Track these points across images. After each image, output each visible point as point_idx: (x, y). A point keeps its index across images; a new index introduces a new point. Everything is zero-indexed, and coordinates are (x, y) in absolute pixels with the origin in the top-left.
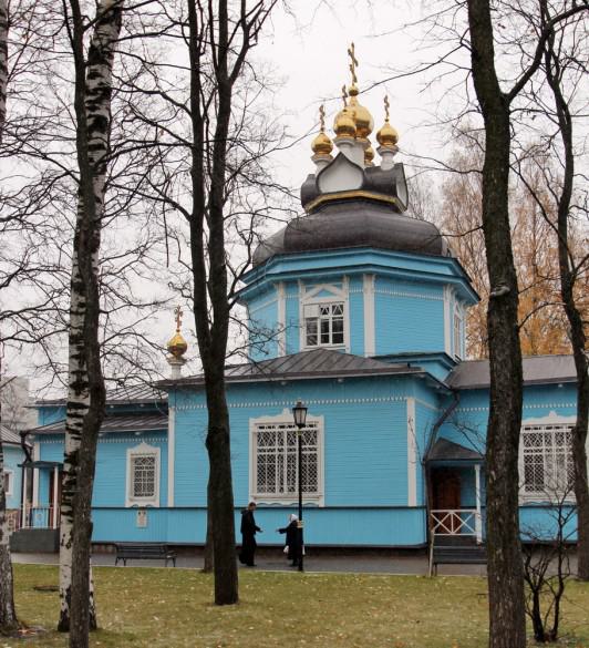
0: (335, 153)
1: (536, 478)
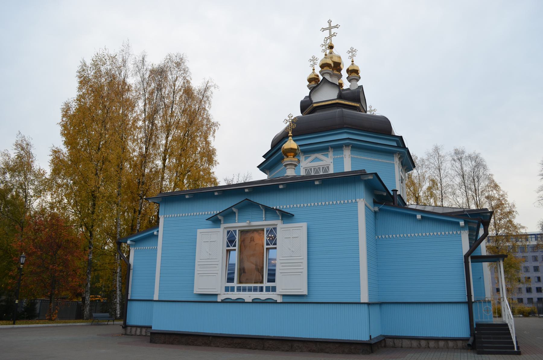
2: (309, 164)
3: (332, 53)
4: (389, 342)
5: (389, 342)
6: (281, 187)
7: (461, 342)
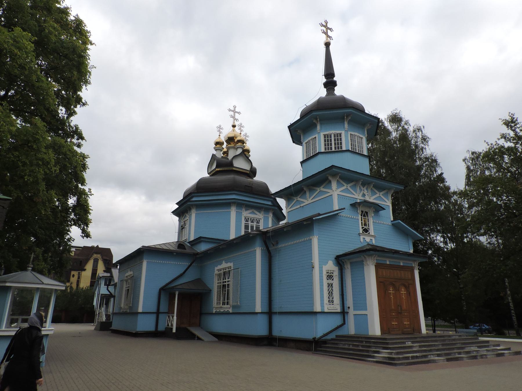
3: (235, 130)
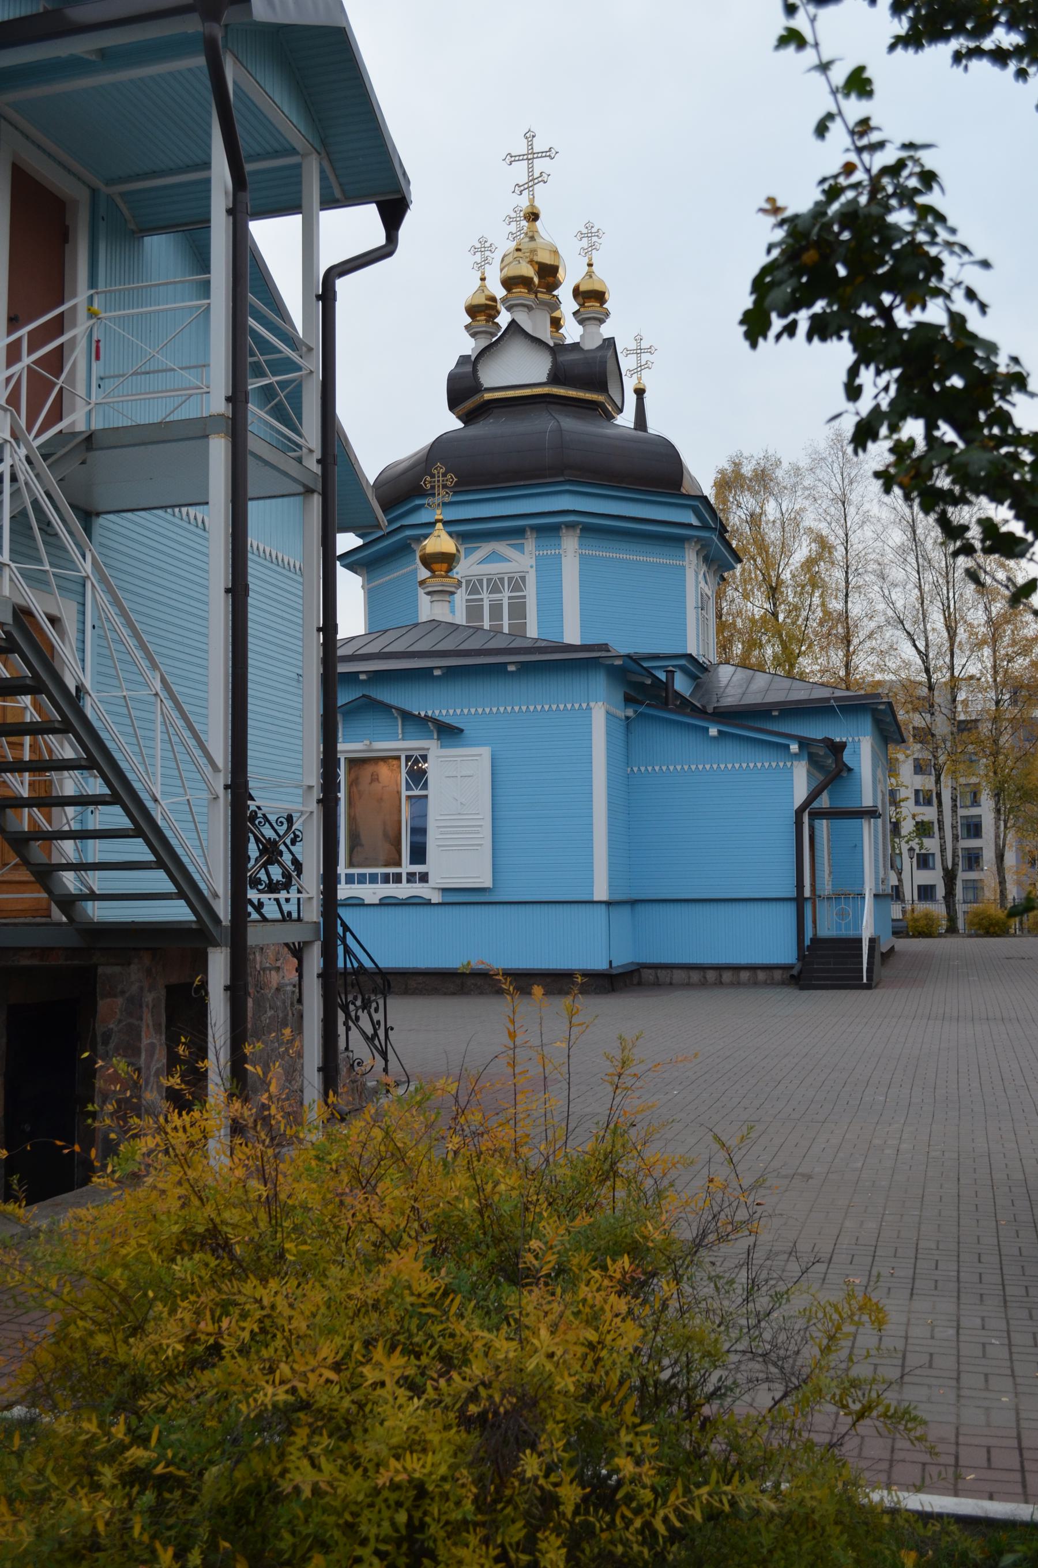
0: (504, 319)
1: (494, 557)
2: (475, 567)
4: (648, 975)
5: (648, 975)
6: (437, 673)
7: (780, 972)
